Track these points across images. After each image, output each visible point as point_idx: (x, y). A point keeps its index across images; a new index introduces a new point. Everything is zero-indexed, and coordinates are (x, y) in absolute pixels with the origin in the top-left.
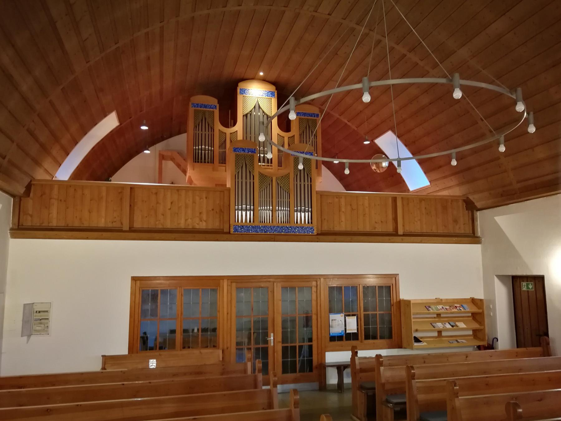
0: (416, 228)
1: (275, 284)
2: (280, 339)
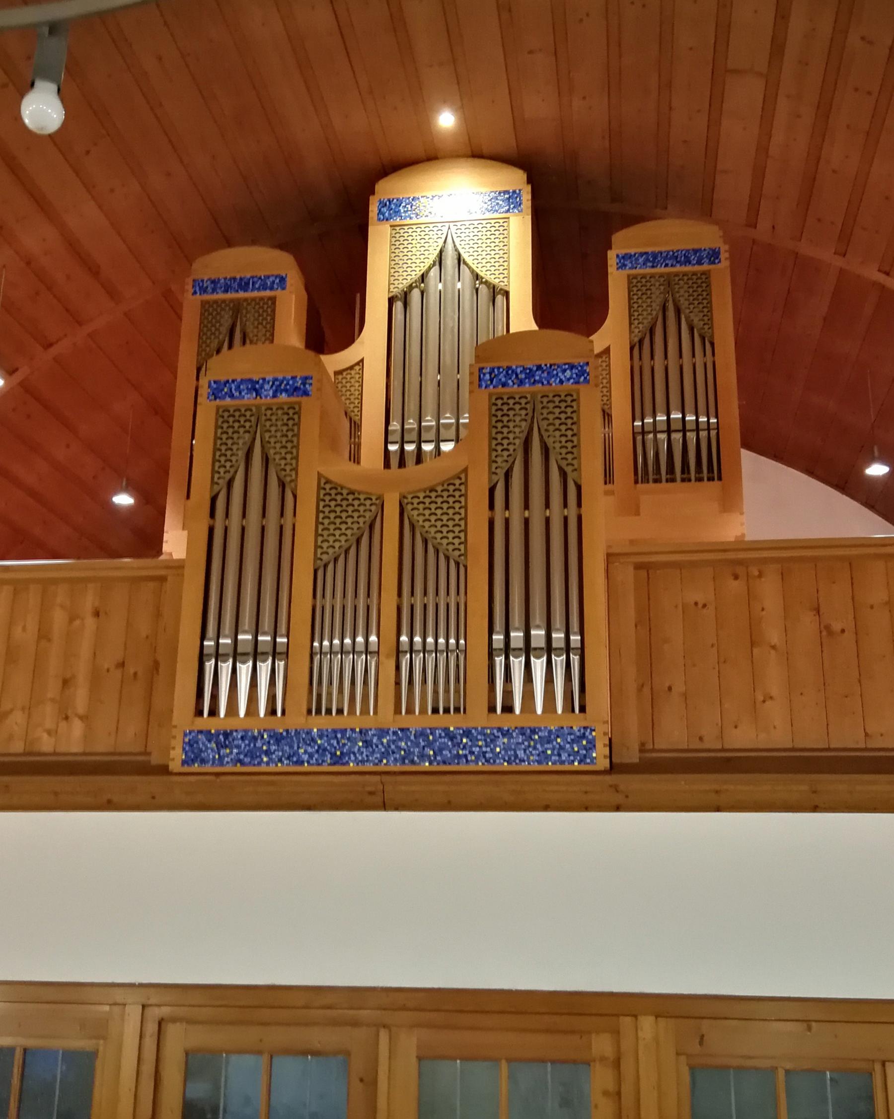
1: (384, 1036)
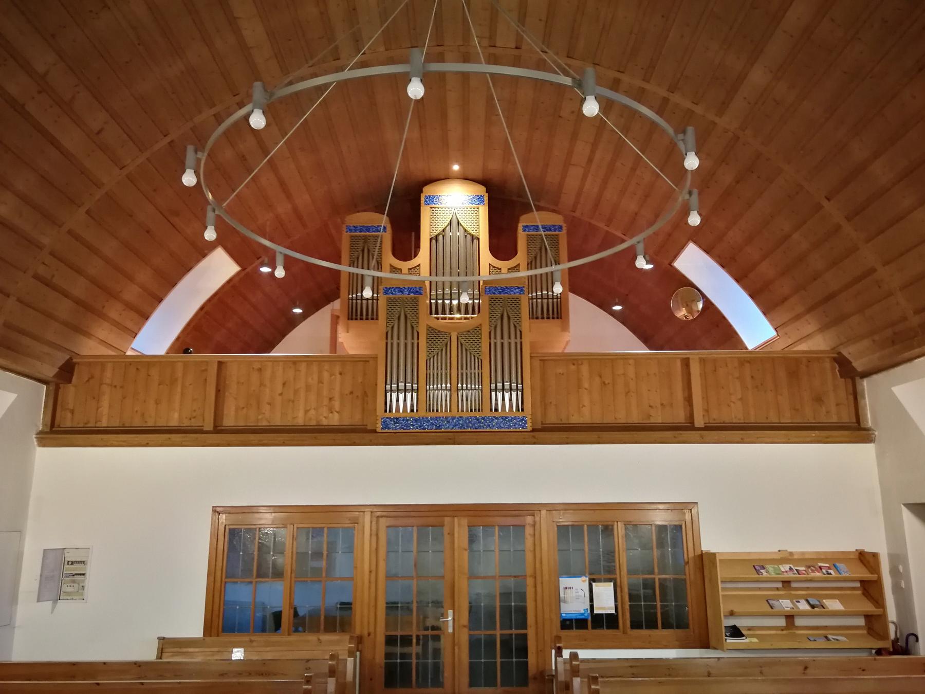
0: (735, 414)
2: (465, 619)
